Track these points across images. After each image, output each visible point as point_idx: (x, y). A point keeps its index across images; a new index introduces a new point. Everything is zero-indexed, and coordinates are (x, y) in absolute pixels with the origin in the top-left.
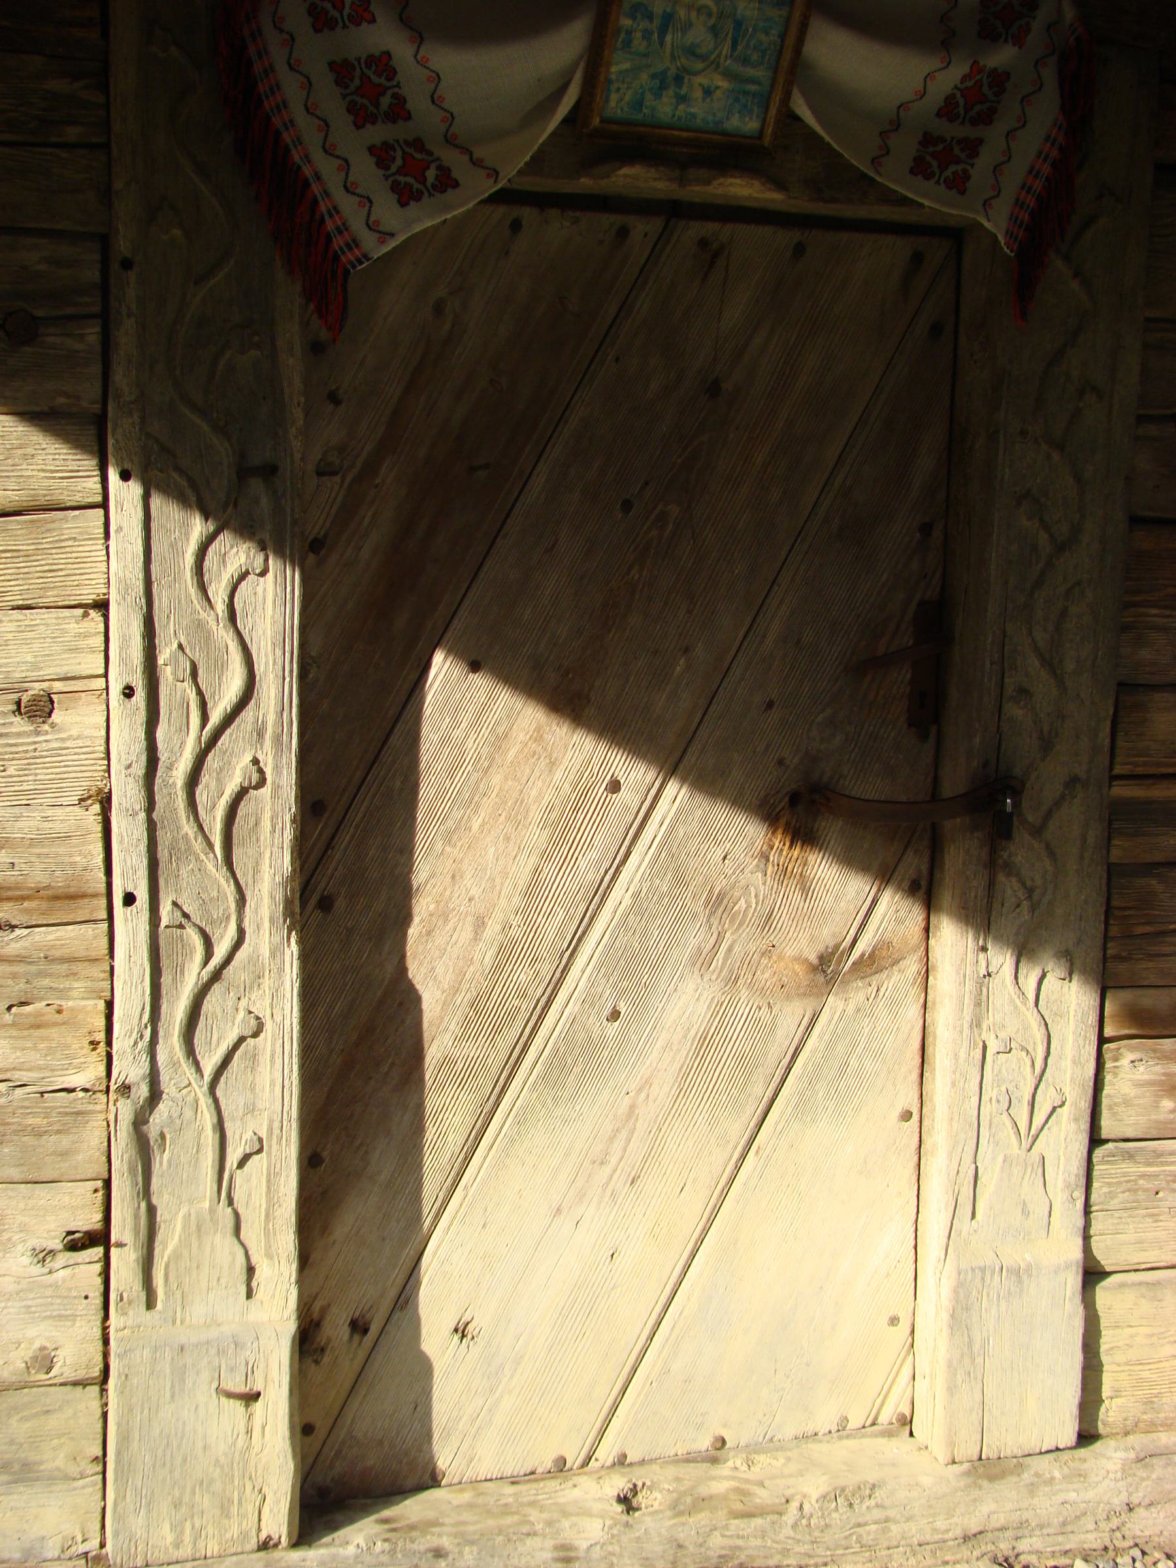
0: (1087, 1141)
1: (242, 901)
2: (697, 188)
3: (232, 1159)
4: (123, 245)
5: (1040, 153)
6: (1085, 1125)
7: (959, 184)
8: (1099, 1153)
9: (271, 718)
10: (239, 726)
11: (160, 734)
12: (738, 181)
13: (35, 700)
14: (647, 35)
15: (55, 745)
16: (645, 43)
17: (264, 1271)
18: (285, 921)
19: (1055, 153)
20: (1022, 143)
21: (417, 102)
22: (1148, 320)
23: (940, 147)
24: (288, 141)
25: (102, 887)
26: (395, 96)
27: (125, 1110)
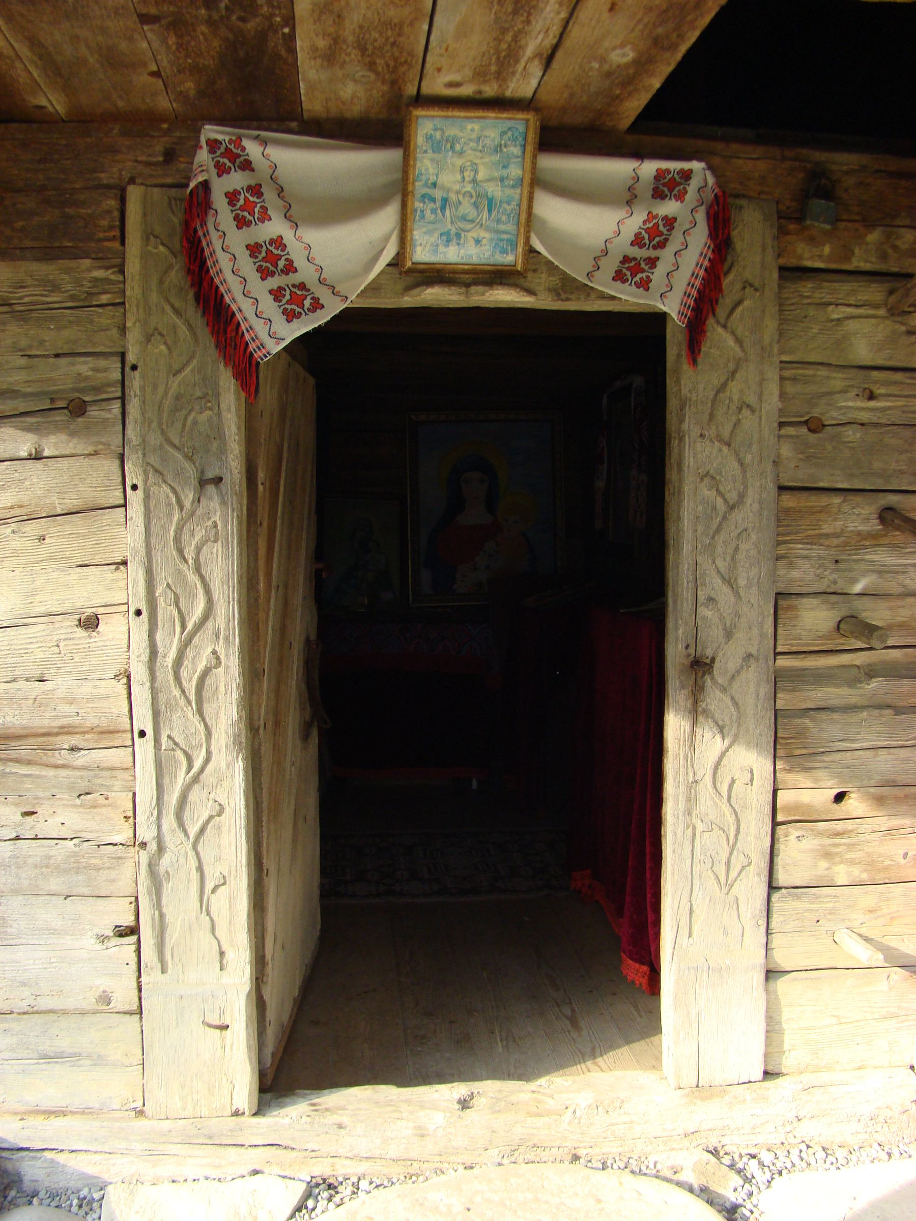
0: (766, 888)
1: (209, 734)
2: (477, 298)
3: (209, 886)
4: (131, 358)
5: (698, 264)
6: (765, 878)
7: (645, 284)
8: (776, 896)
9: (223, 626)
10: (204, 632)
11: (158, 637)
12: (501, 292)
13: (88, 618)
14: (434, 211)
15: (100, 644)
16: (433, 216)
17: (230, 955)
18: (234, 747)
19: (706, 263)
20: (690, 251)
21: (300, 262)
22: (781, 362)
23: (633, 264)
24: (223, 291)
25: (128, 727)
26: (287, 260)
27: (144, 857)
